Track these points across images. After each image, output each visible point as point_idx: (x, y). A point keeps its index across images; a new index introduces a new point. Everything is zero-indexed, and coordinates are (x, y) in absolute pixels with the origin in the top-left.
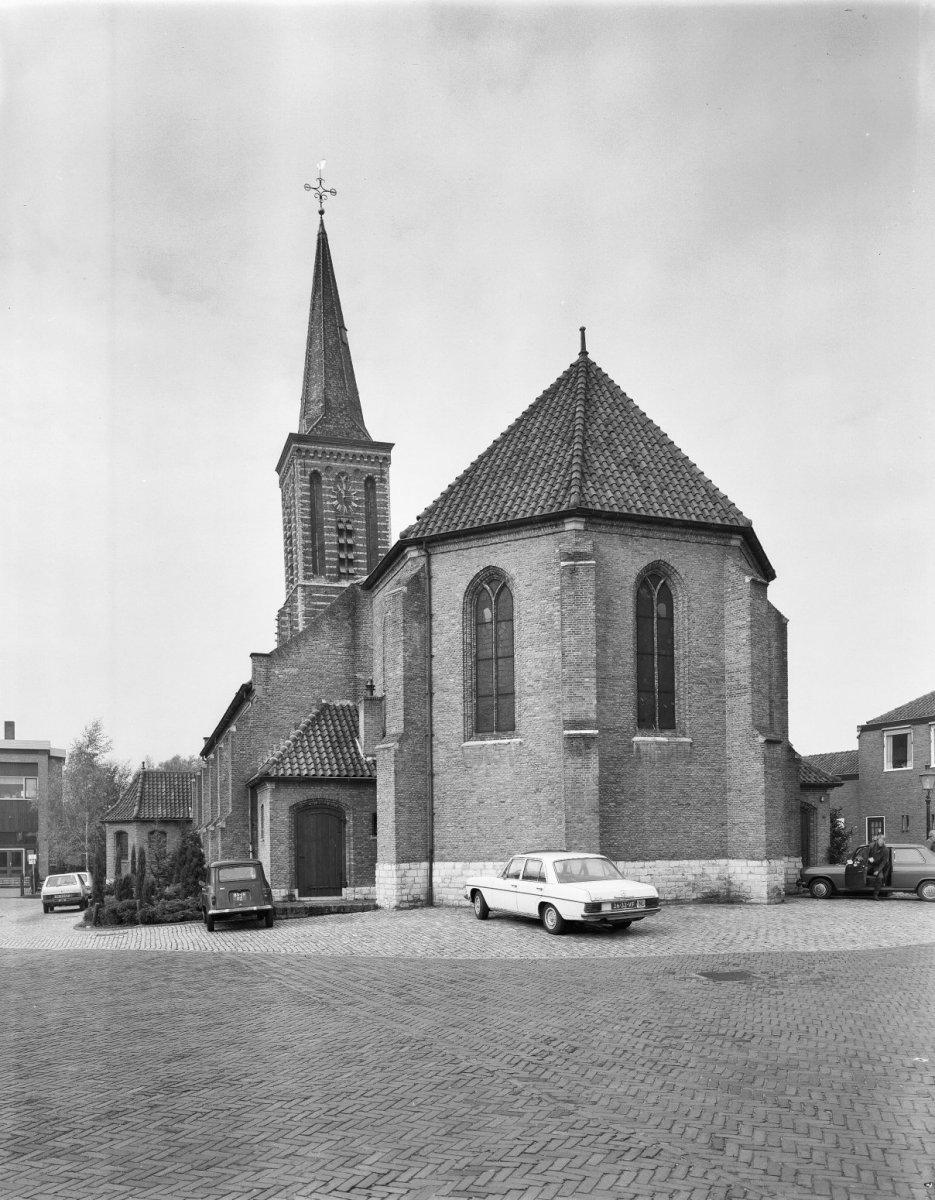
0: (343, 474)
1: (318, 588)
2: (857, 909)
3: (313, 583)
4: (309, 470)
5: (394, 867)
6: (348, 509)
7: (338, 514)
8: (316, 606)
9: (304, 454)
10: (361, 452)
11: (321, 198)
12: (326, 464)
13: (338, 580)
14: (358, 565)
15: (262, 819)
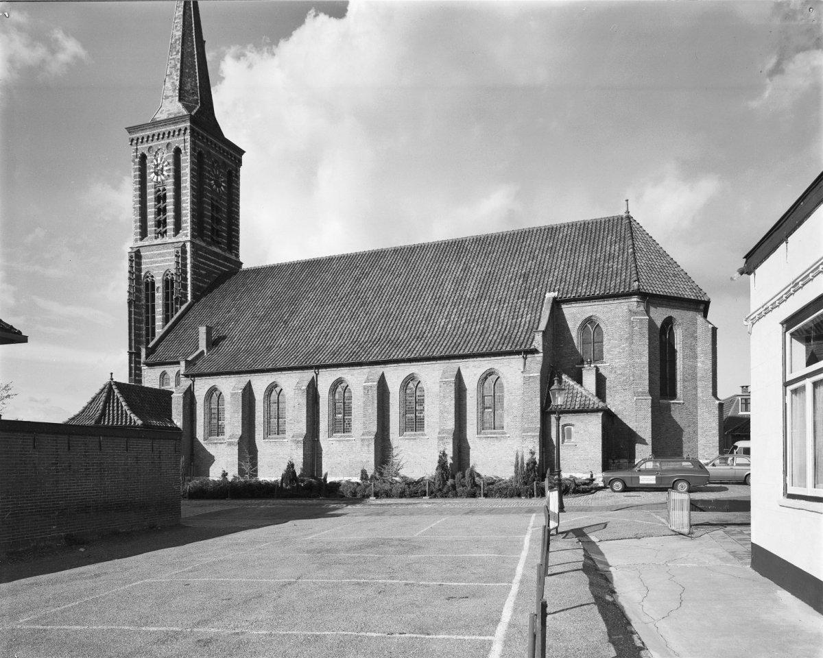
0: (216, 161)
1: (201, 248)
3: (197, 242)
7: (213, 191)
10: (227, 149)
14: (222, 237)
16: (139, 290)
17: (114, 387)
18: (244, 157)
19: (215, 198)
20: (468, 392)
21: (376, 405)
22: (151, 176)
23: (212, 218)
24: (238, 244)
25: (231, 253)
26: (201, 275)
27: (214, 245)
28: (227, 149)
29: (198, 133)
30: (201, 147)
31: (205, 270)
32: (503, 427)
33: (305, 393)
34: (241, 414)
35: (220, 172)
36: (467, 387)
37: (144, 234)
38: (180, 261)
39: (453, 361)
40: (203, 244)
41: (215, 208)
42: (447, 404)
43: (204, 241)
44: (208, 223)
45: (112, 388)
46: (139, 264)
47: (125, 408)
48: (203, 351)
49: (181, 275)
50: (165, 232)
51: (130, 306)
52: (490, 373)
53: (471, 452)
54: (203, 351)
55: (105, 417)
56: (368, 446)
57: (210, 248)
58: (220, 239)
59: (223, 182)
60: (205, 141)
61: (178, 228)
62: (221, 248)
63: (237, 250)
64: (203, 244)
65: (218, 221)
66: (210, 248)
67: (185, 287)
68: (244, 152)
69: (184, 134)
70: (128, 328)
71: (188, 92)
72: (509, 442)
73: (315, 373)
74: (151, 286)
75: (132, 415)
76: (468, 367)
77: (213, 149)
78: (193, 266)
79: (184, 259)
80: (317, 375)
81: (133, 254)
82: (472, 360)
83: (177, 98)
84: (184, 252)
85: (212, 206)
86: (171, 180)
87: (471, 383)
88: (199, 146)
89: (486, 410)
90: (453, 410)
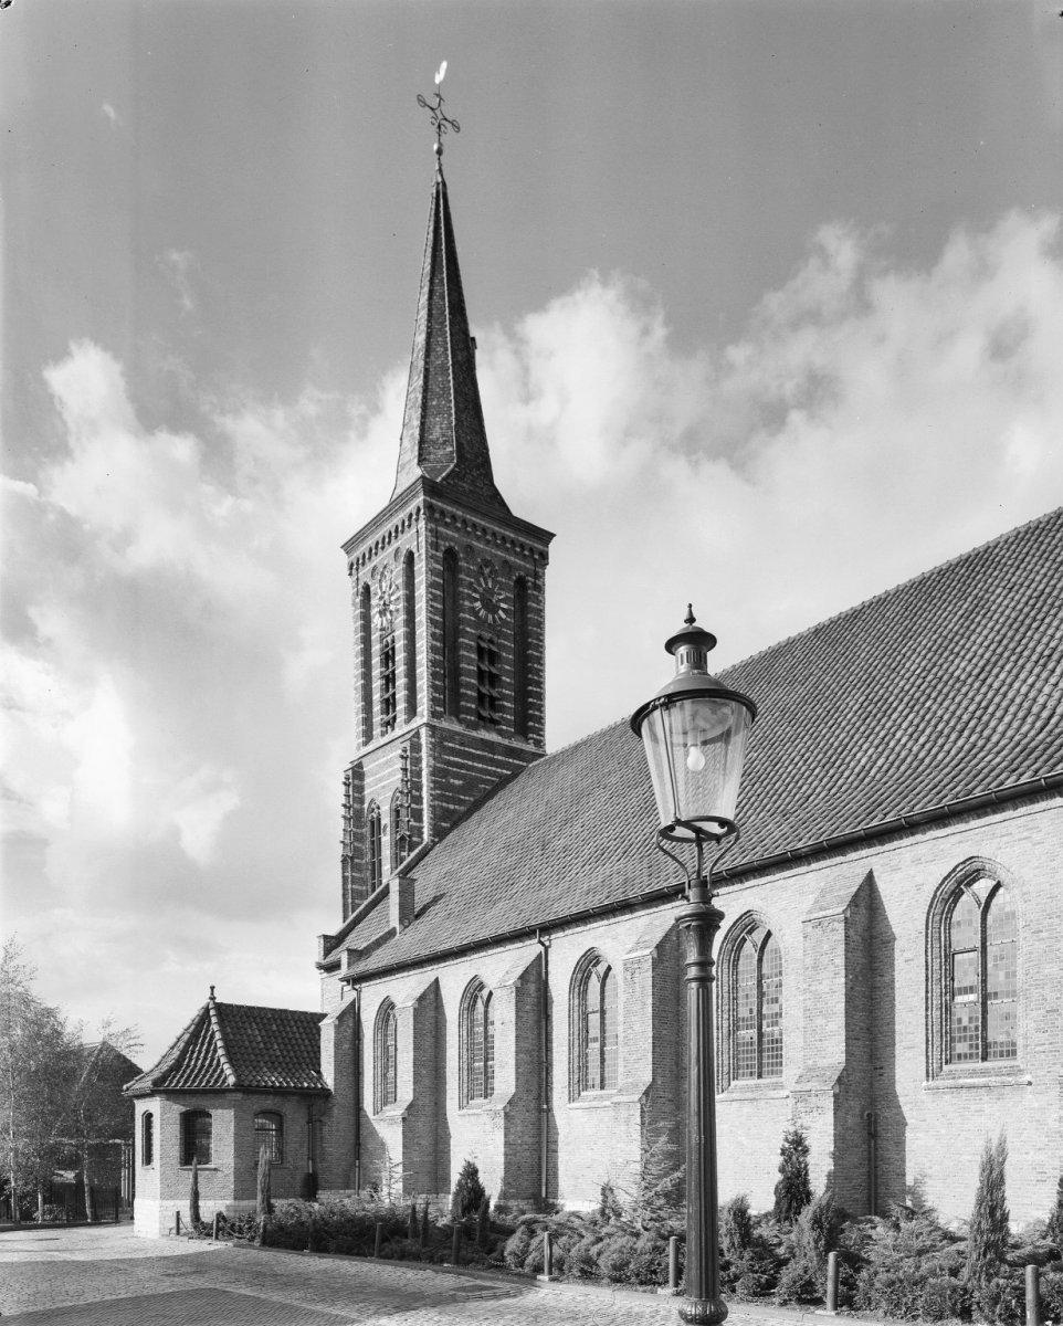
0: (487, 563)
1: (452, 736)
2: (423, 1289)
3: (445, 724)
4: (444, 545)
5: (158, 1202)
6: (494, 618)
7: (480, 623)
8: (449, 763)
9: (437, 515)
10: (512, 535)
11: (439, 127)
12: (466, 540)
13: (475, 727)
14: (502, 709)
15: (698, 1061)
16: (359, 838)
17: (212, 1012)
18: (553, 549)
19: (487, 635)
20: (898, 945)
21: (650, 1009)
22: (377, 621)
23: (481, 675)
24: (540, 720)
25: (527, 739)
26: (452, 788)
27: (485, 728)
28: (512, 535)
29: (443, 513)
30: (452, 539)
31: (457, 776)
32: (1014, 1053)
33: (514, 994)
34: (412, 1054)
35: (495, 582)
36: (896, 930)
37: (368, 735)
38: (408, 767)
39: (853, 855)
40: (458, 728)
41: (487, 654)
42: (824, 988)
43: (460, 721)
44: (469, 686)
45: (209, 1017)
46: (360, 789)
47: (220, 1052)
48: (394, 928)
49: (410, 792)
50: (394, 718)
51: (344, 869)
52: (968, 875)
53: (909, 1135)
54: (394, 928)
55: (178, 1072)
56: (627, 1122)
57: (474, 734)
58: (497, 716)
59: (504, 601)
60: (509, 545)
61: (412, 710)
62: (500, 732)
63: (540, 731)
64: (458, 728)
65: (494, 680)
66: (474, 734)
67: (418, 815)
68: (553, 535)
69: (417, 520)
70: (341, 909)
71: (434, 442)
72: (1030, 1098)
73: (543, 944)
74: (376, 825)
75: (226, 1066)
76: (896, 869)
77: (478, 539)
78: (435, 772)
79: (417, 761)
80: (546, 948)
81: (350, 773)
82: (911, 840)
83: (416, 460)
84: (416, 747)
85: (480, 651)
86: (401, 617)
87: (905, 914)
88: (446, 538)
89: (959, 999)
90: (841, 1006)
